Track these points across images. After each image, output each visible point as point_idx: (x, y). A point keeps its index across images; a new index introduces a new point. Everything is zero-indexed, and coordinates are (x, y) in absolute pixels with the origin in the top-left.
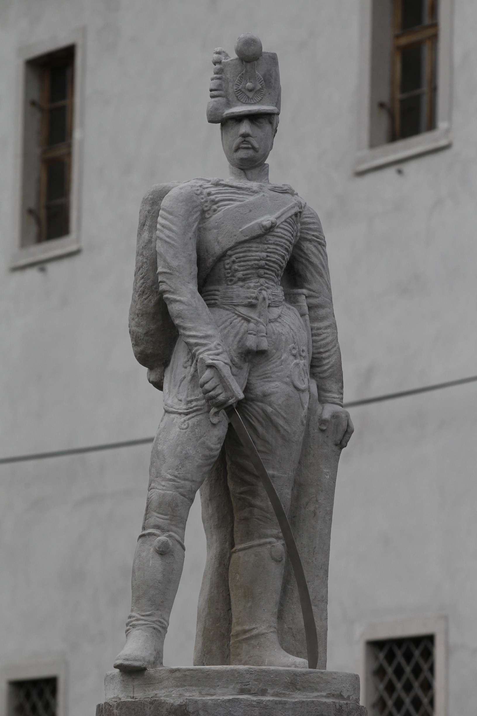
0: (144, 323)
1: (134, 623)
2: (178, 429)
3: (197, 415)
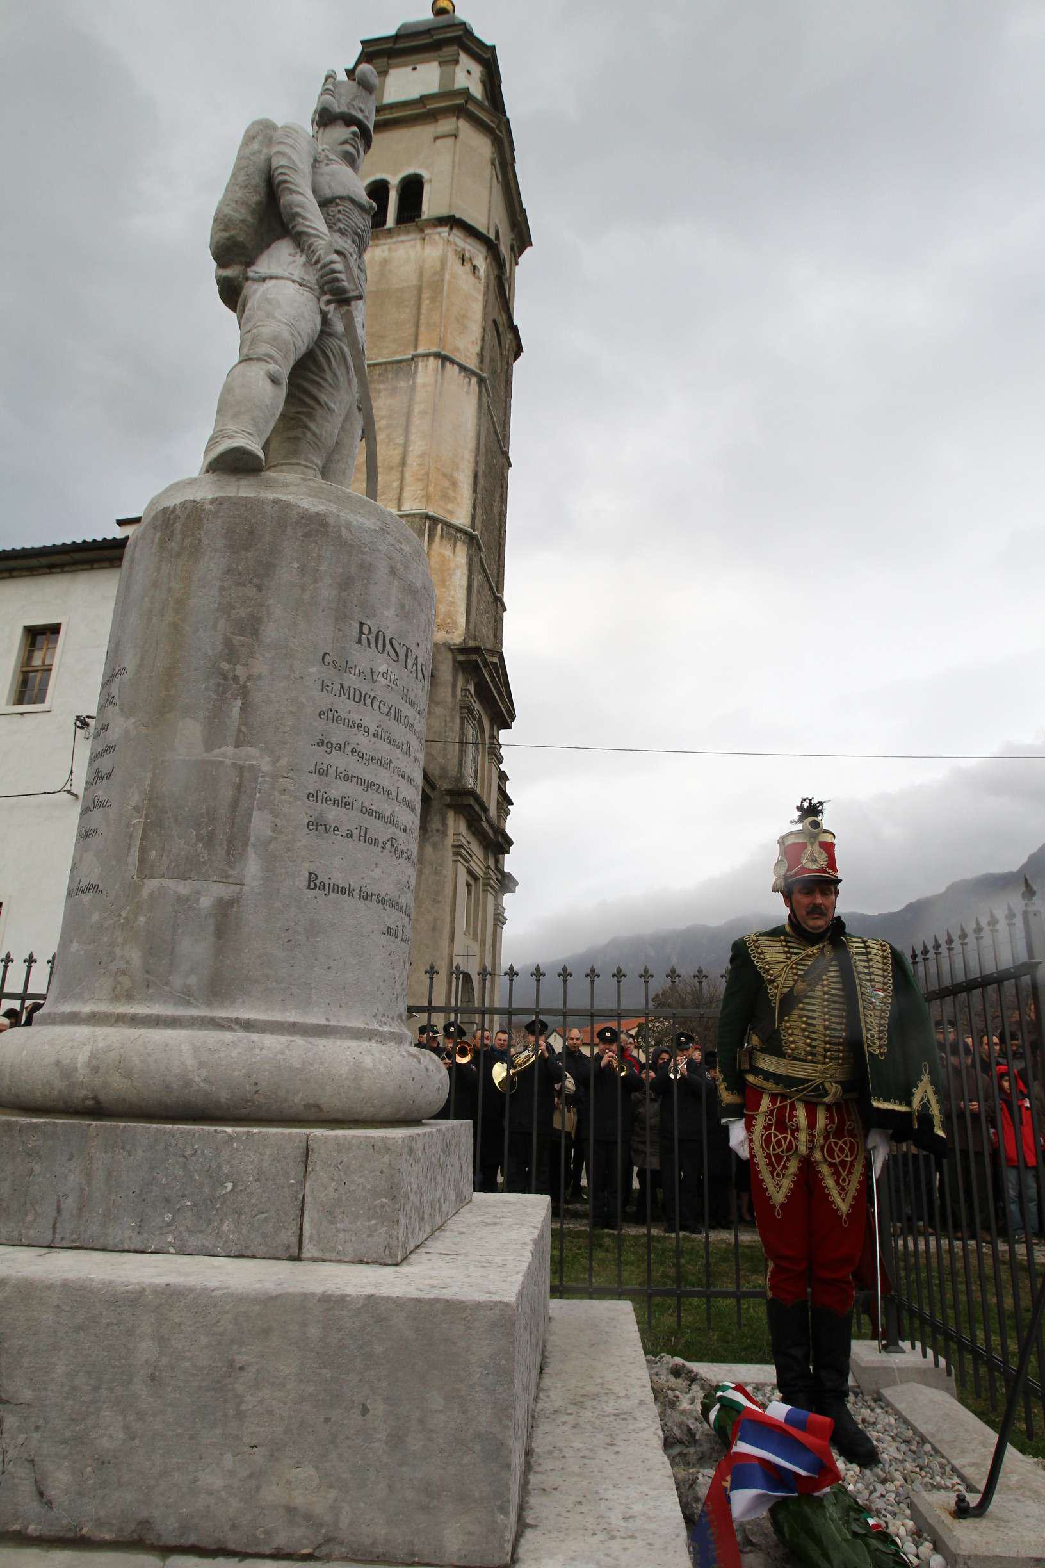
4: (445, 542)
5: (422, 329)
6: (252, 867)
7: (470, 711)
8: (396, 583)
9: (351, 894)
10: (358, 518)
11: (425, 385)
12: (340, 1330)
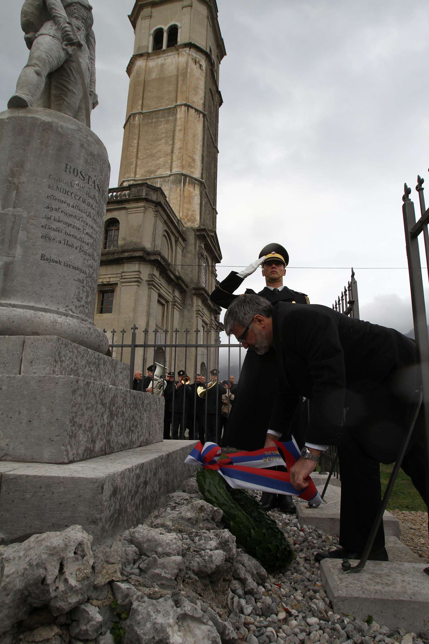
5: (179, 94)
6: (19, 251)
7: (202, 255)
8: (83, 150)
9: (60, 263)
10: (67, 125)
11: (181, 118)
12: (13, 387)
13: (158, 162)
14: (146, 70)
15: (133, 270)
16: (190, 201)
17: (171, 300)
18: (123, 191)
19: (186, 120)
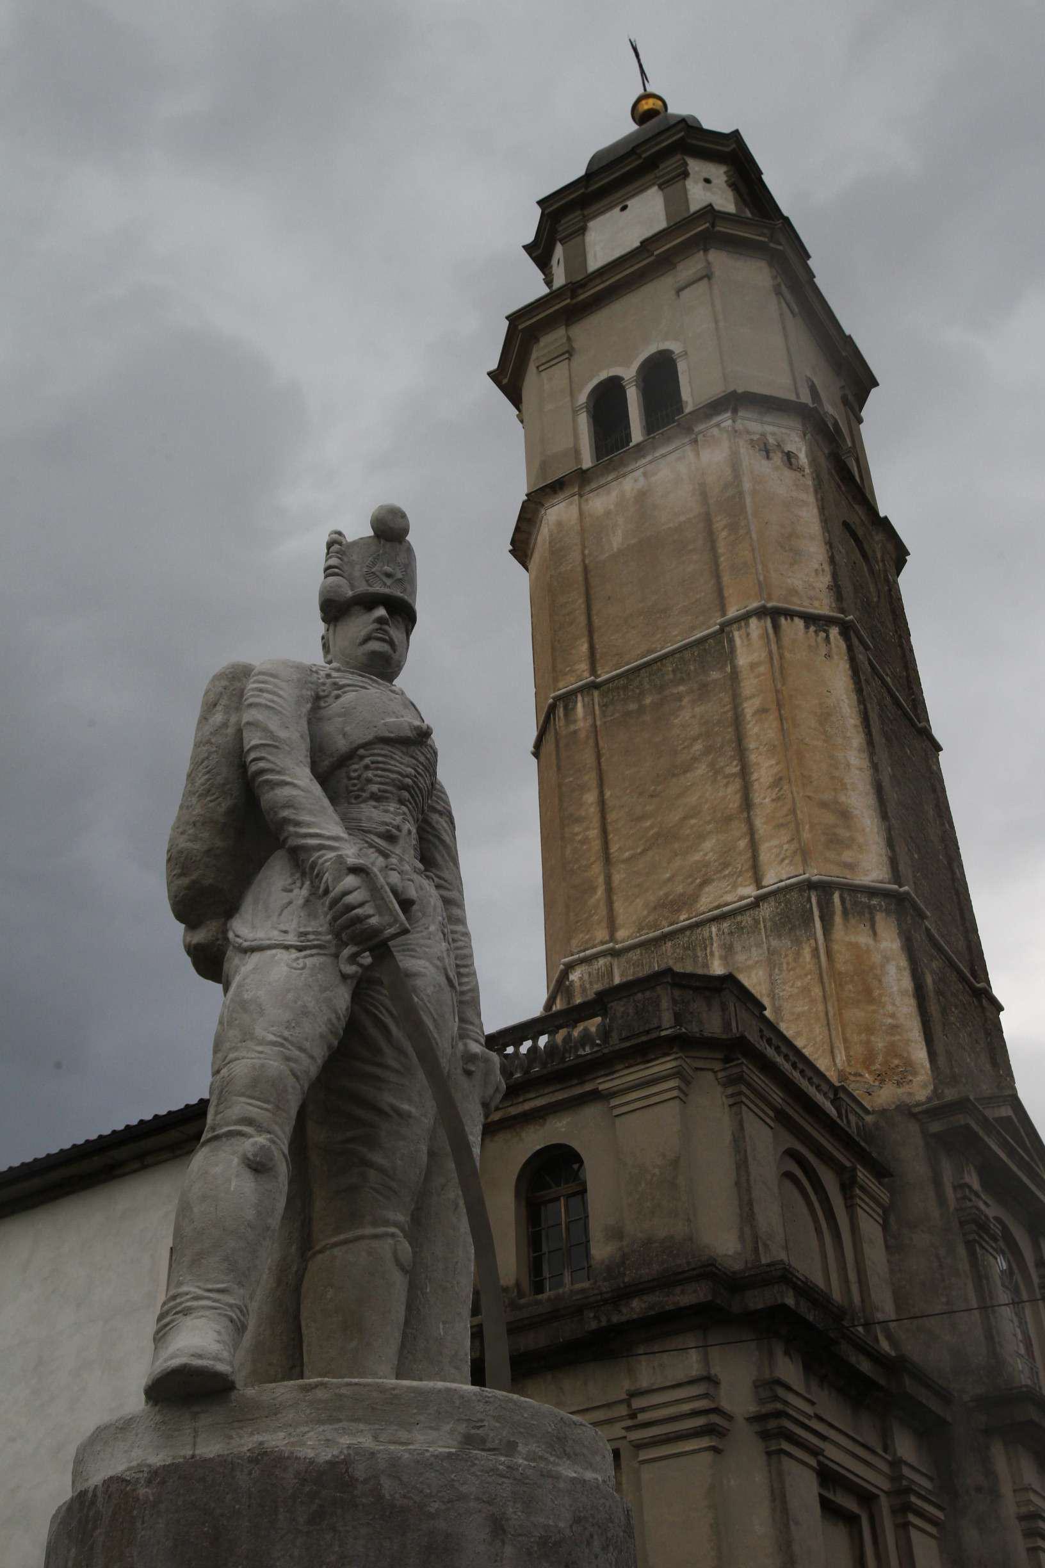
0: (206, 835)
1: (189, 1304)
2: (285, 969)
3: (318, 954)
4: (853, 921)
5: (726, 579)
7: (982, 1226)
11: (753, 666)
13: (697, 857)
14: (583, 530)
15: (681, 1376)
16: (868, 991)
17: (886, 1485)
18: (576, 1023)
19: (779, 667)
